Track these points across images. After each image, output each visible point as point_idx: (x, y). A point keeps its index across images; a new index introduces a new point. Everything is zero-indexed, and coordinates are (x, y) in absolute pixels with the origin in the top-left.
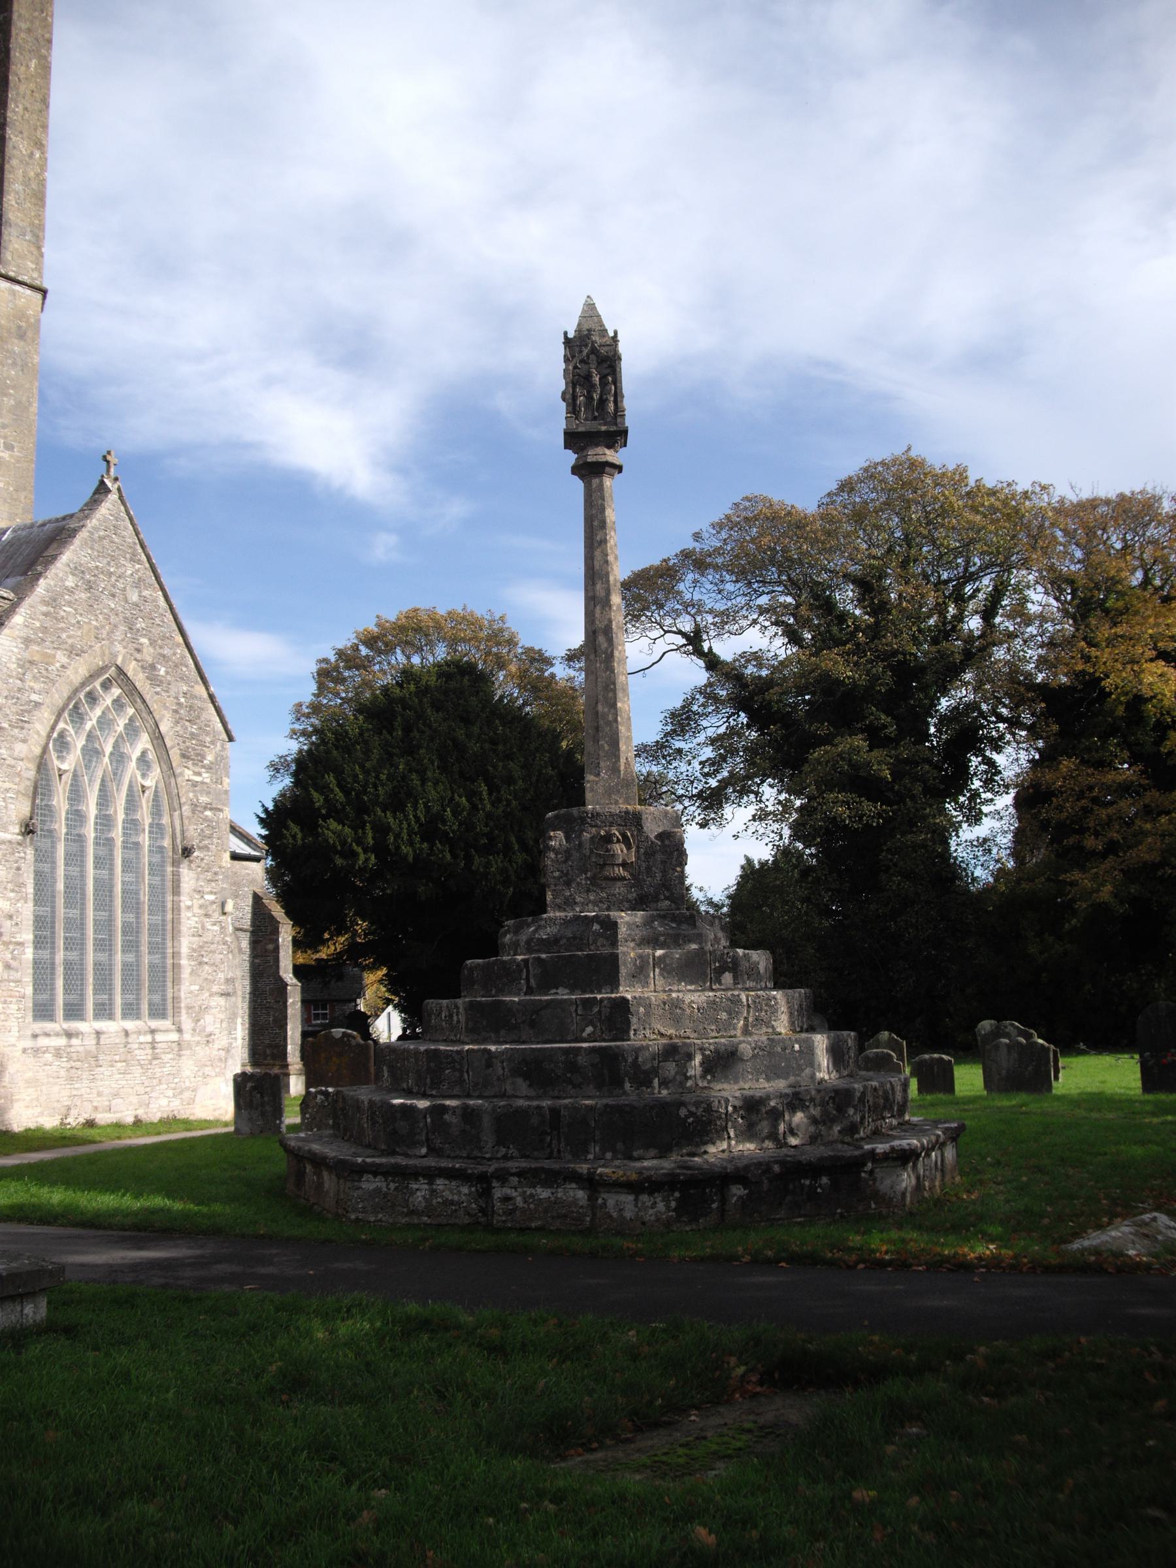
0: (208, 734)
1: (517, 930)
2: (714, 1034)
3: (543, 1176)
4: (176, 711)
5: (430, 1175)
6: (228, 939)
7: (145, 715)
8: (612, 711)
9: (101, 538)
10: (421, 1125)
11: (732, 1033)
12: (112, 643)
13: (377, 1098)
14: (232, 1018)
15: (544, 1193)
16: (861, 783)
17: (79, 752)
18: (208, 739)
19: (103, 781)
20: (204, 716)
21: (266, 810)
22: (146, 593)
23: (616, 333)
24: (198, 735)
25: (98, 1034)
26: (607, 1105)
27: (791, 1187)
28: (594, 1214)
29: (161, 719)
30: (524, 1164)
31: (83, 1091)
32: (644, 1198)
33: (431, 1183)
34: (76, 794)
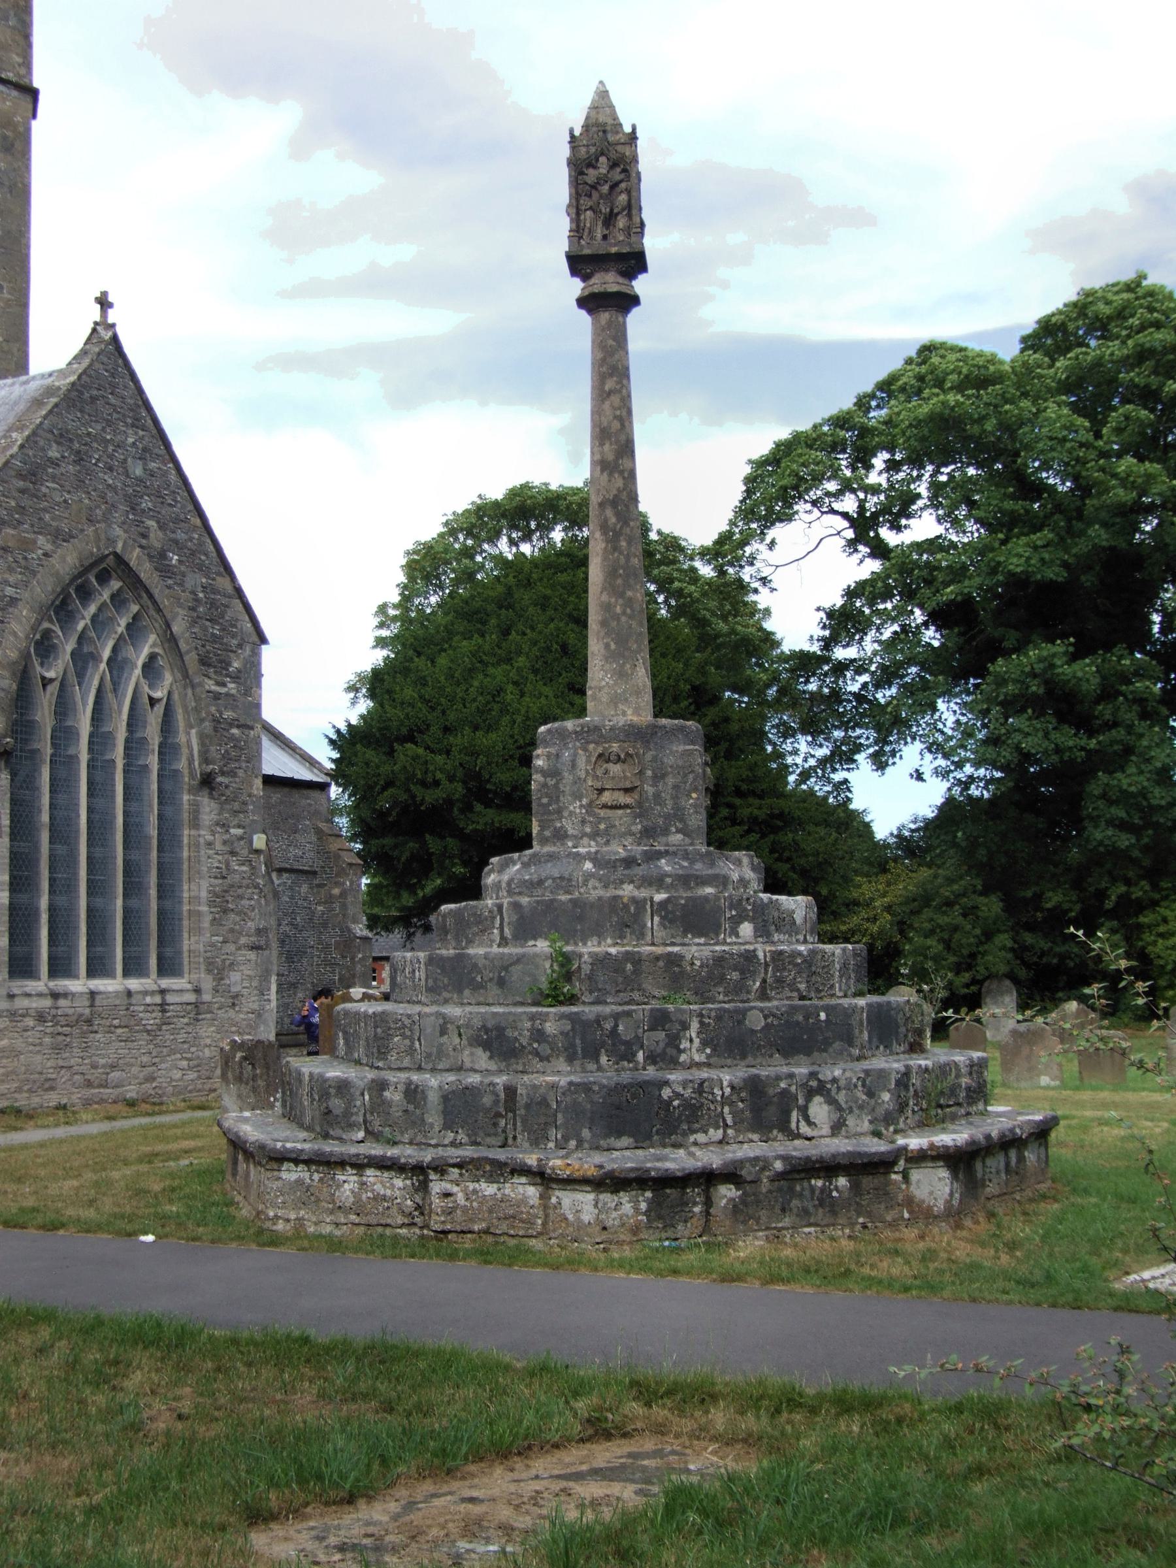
0: (234, 636)
1: (502, 868)
2: (721, 997)
3: (488, 1168)
4: (193, 609)
5: (359, 1165)
6: (260, 881)
7: (152, 612)
9: (94, 399)
10: (358, 1103)
11: (744, 996)
12: (110, 526)
13: (317, 1071)
14: (265, 977)
15: (489, 1189)
16: (1062, 704)
17: (68, 657)
18: (235, 642)
19: (99, 691)
21: (338, 732)
22: (153, 465)
23: (634, 128)
24: (221, 638)
25: (93, 994)
26: (571, 1083)
27: (798, 1188)
28: (547, 1216)
29: (174, 618)
30: (469, 1152)
31: (72, 1062)
32: (606, 1197)
34: (63, 707)
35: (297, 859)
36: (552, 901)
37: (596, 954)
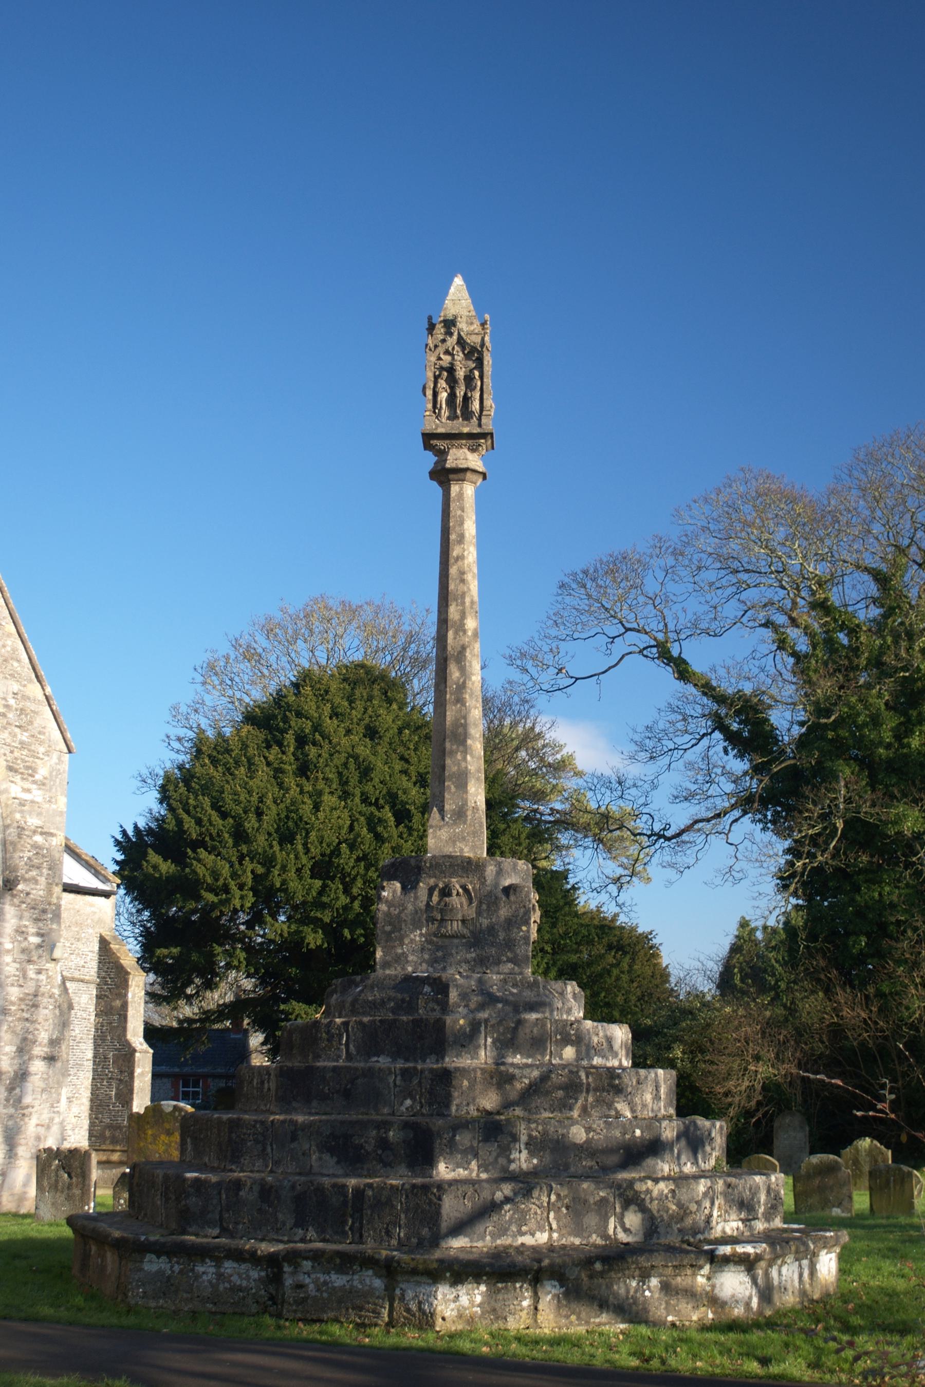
0: (41, 743)
1: (345, 990)
8: (461, 748)
18: (42, 750)
20: (38, 722)
33: (218, 1266)
35: (78, 968)
36: (395, 1021)
37: (436, 1070)
